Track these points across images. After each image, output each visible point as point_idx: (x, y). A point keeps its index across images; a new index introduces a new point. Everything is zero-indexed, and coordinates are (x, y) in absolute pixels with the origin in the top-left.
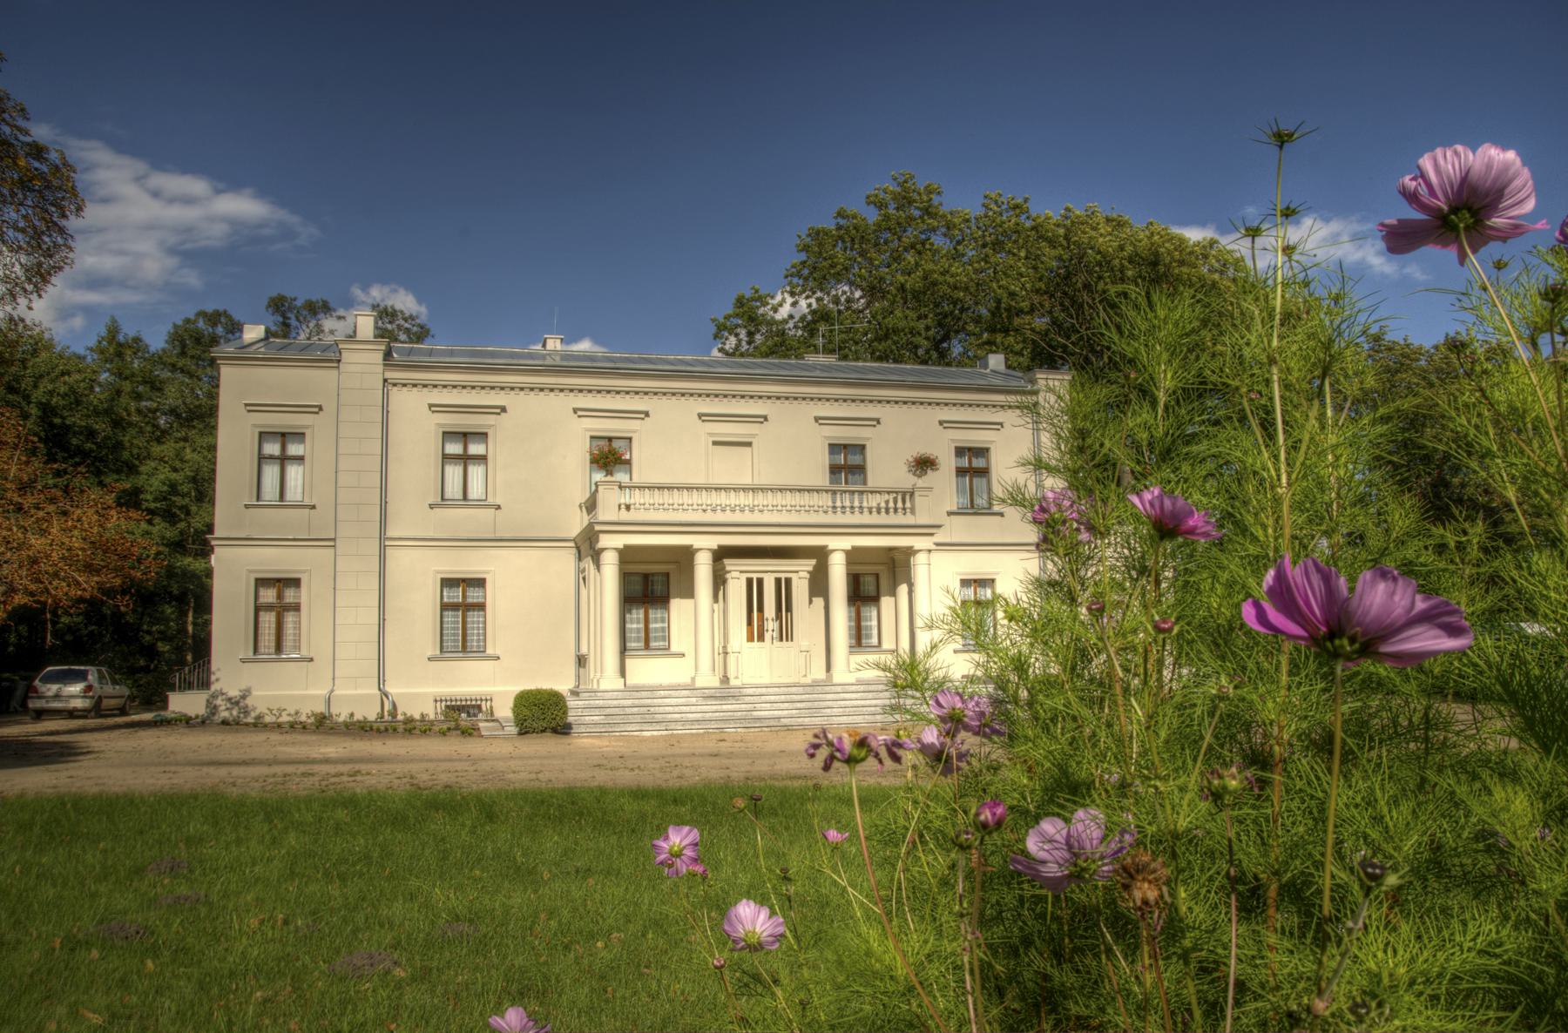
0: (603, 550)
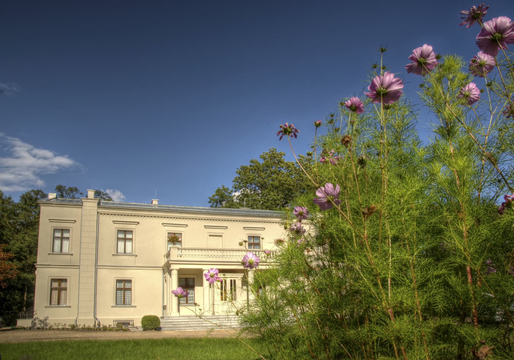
0: (172, 270)
